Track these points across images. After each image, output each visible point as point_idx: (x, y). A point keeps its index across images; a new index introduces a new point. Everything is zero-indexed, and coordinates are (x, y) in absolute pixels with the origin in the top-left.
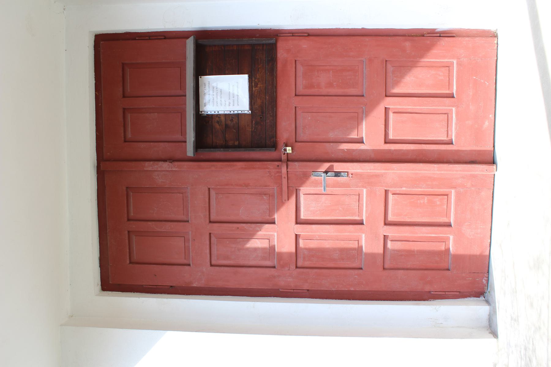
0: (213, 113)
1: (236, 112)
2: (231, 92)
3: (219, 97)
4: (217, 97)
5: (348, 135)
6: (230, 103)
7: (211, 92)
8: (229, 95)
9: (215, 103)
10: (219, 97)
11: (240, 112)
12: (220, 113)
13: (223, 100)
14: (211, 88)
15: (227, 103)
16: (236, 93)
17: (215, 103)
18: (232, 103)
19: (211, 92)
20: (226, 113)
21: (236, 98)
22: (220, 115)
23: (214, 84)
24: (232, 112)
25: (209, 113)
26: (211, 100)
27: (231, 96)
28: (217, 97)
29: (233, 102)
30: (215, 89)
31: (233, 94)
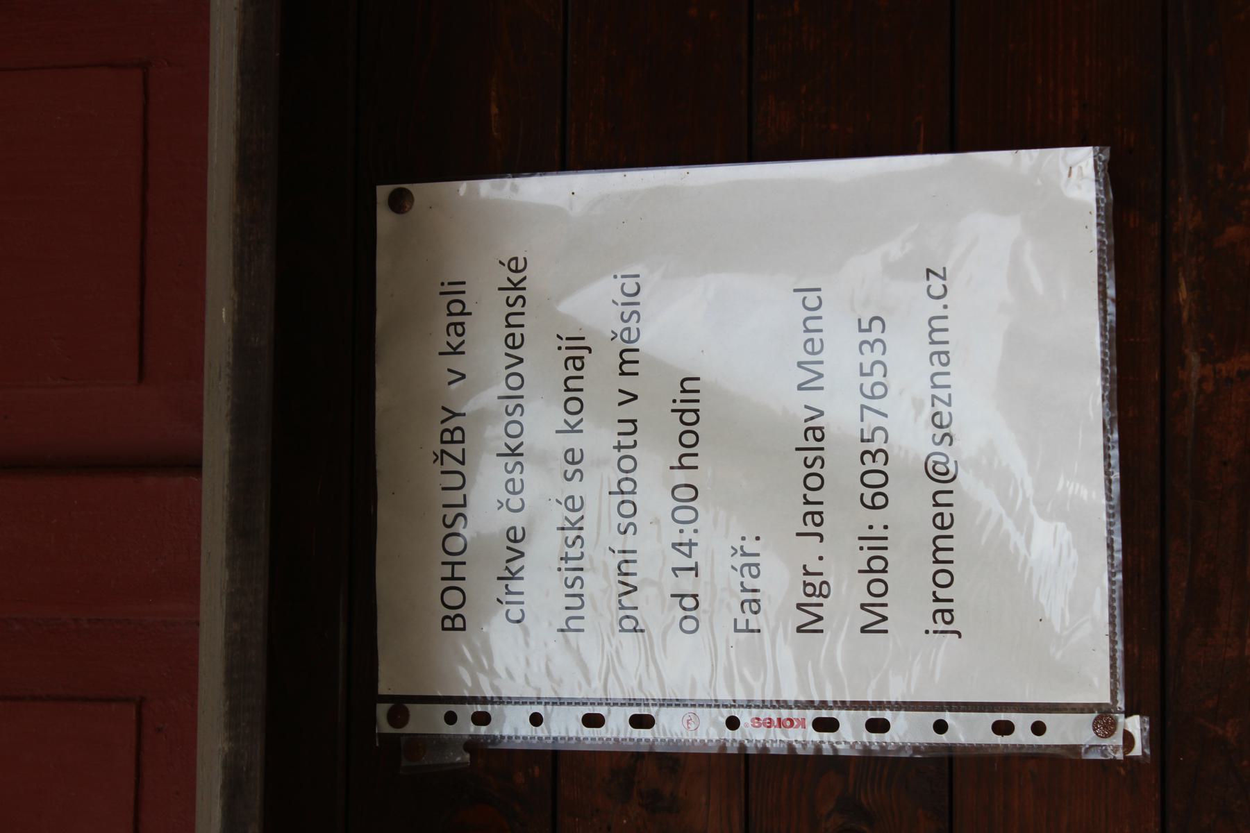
0: (564, 727)
1: (907, 731)
2: (842, 416)
3: (654, 497)
4: (624, 493)
5: (1042, 515)
6: (815, 589)
7: (542, 421)
8: (814, 479)
9: (599, 585)
10: (654, 497)
11: (970, 731)
12: (673, 729)
13: (716, 542)
14: (543, 364)
15: (779, 584)
16: (910, 439)
17: (599, 585)
18: (847, 590)
19: (542, 421)
20: (755, 734)
21: (910, 506)
22: (673, 762)
23: (592, 306)
24: (851, 734)
25: (512, 726)
26: (543, 550)
27: (842, 470)
28: (624, 493)
29: (875, 569)
30: (602, 365)
31: (874, 456)
